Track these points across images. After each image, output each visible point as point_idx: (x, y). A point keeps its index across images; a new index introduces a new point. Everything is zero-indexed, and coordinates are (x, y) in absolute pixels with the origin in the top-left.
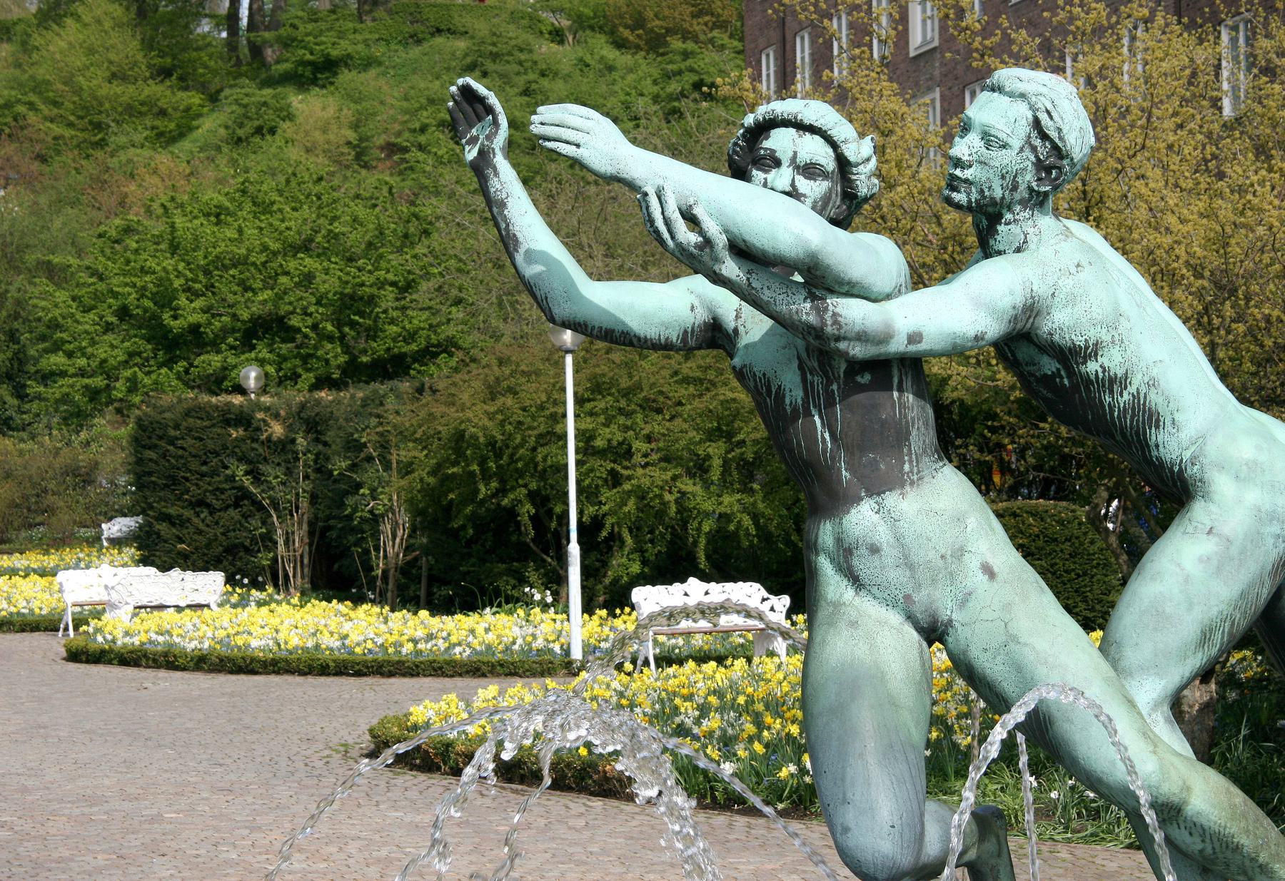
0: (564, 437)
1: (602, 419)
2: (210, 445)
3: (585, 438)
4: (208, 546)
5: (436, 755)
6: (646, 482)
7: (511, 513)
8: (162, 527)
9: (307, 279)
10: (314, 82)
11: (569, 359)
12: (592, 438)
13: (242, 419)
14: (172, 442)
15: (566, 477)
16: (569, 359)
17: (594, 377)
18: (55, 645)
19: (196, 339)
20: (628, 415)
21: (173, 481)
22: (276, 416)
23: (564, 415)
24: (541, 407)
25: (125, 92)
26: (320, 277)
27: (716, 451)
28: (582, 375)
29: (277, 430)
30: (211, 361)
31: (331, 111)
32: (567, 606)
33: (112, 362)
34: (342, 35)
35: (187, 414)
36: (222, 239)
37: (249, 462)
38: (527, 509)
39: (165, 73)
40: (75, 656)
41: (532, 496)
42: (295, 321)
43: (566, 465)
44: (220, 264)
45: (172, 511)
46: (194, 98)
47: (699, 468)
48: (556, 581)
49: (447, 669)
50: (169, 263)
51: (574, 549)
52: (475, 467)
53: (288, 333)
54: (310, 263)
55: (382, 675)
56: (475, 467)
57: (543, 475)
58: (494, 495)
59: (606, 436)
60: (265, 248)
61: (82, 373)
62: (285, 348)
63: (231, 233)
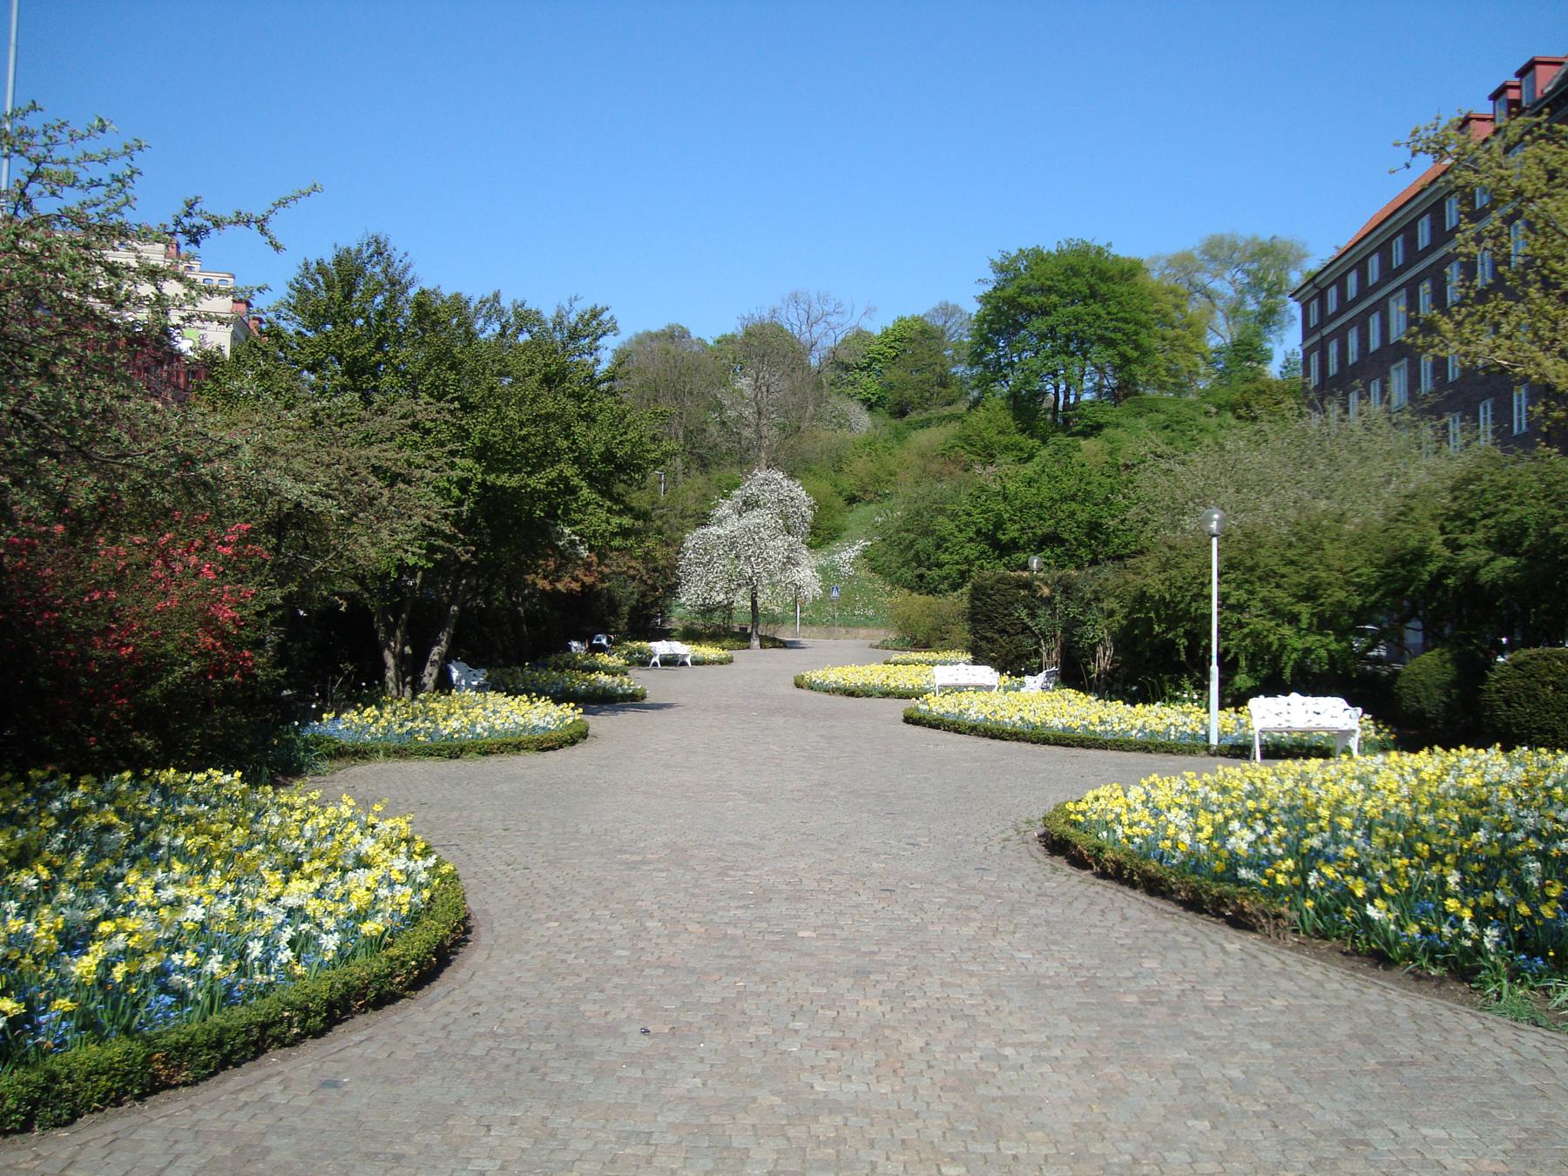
0: (1209, 597)
1: (1234, 585)
2: (1009, 599)
3: (1223, 598)
4: (1007, 655)
5: (1089, 856)
6: (1259, 627)
7: (1173, 643)
8: (983, 644)
9: (1073, 514)
10: (1091, 435)
11: (1215, 540)
12: (1227, 598)
13: (1027, 585)
14: (989, 596)
15: (1210, 623)
16: (1215, 540)
17: (1229, 559)
18: (900, 707)
19: (1013, 546)
20: (1252, 583)
21: (989, 619)
22: (1046, 584)
23: (1210, 582)
24: (1195, 578)
25: (1005, 440)
26: (1079, 513)
27: (1304, 610)
28: (1222, 558)
29: (1046, 591)
30: (1021, 557)
31: (1099, 447)
32: (1208, 703)
33: (972, 557)
34: (1105, 412)
35: (998, 581)
36: (1029, 495)
37: (1030, 609)
38: (1183, 642)
39: (1023, 431)
40: (909, 720)
41: (1187, 634)
42: (1066, 536)
43: (1210, 615)
44: (1028, 507)
45: (988, 635)
46: (1037, 442)
47: (1294, 619)
48: (1202, 686)
49: (1125, 746)
50: (1002, 506)
51: (1214, 669)
52: (1152, 615)
53: (1062, 542)
54: (1074, 506)
55: (1083, 747)
56: (1152, 615)
57: (1195, 620)
58: (1163, 632)
59: (1237, 596)
60: (1052, 499)
61: (957, 563)
62: (1058, 551)
63: (1034, 491)
